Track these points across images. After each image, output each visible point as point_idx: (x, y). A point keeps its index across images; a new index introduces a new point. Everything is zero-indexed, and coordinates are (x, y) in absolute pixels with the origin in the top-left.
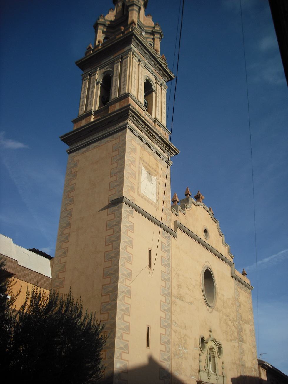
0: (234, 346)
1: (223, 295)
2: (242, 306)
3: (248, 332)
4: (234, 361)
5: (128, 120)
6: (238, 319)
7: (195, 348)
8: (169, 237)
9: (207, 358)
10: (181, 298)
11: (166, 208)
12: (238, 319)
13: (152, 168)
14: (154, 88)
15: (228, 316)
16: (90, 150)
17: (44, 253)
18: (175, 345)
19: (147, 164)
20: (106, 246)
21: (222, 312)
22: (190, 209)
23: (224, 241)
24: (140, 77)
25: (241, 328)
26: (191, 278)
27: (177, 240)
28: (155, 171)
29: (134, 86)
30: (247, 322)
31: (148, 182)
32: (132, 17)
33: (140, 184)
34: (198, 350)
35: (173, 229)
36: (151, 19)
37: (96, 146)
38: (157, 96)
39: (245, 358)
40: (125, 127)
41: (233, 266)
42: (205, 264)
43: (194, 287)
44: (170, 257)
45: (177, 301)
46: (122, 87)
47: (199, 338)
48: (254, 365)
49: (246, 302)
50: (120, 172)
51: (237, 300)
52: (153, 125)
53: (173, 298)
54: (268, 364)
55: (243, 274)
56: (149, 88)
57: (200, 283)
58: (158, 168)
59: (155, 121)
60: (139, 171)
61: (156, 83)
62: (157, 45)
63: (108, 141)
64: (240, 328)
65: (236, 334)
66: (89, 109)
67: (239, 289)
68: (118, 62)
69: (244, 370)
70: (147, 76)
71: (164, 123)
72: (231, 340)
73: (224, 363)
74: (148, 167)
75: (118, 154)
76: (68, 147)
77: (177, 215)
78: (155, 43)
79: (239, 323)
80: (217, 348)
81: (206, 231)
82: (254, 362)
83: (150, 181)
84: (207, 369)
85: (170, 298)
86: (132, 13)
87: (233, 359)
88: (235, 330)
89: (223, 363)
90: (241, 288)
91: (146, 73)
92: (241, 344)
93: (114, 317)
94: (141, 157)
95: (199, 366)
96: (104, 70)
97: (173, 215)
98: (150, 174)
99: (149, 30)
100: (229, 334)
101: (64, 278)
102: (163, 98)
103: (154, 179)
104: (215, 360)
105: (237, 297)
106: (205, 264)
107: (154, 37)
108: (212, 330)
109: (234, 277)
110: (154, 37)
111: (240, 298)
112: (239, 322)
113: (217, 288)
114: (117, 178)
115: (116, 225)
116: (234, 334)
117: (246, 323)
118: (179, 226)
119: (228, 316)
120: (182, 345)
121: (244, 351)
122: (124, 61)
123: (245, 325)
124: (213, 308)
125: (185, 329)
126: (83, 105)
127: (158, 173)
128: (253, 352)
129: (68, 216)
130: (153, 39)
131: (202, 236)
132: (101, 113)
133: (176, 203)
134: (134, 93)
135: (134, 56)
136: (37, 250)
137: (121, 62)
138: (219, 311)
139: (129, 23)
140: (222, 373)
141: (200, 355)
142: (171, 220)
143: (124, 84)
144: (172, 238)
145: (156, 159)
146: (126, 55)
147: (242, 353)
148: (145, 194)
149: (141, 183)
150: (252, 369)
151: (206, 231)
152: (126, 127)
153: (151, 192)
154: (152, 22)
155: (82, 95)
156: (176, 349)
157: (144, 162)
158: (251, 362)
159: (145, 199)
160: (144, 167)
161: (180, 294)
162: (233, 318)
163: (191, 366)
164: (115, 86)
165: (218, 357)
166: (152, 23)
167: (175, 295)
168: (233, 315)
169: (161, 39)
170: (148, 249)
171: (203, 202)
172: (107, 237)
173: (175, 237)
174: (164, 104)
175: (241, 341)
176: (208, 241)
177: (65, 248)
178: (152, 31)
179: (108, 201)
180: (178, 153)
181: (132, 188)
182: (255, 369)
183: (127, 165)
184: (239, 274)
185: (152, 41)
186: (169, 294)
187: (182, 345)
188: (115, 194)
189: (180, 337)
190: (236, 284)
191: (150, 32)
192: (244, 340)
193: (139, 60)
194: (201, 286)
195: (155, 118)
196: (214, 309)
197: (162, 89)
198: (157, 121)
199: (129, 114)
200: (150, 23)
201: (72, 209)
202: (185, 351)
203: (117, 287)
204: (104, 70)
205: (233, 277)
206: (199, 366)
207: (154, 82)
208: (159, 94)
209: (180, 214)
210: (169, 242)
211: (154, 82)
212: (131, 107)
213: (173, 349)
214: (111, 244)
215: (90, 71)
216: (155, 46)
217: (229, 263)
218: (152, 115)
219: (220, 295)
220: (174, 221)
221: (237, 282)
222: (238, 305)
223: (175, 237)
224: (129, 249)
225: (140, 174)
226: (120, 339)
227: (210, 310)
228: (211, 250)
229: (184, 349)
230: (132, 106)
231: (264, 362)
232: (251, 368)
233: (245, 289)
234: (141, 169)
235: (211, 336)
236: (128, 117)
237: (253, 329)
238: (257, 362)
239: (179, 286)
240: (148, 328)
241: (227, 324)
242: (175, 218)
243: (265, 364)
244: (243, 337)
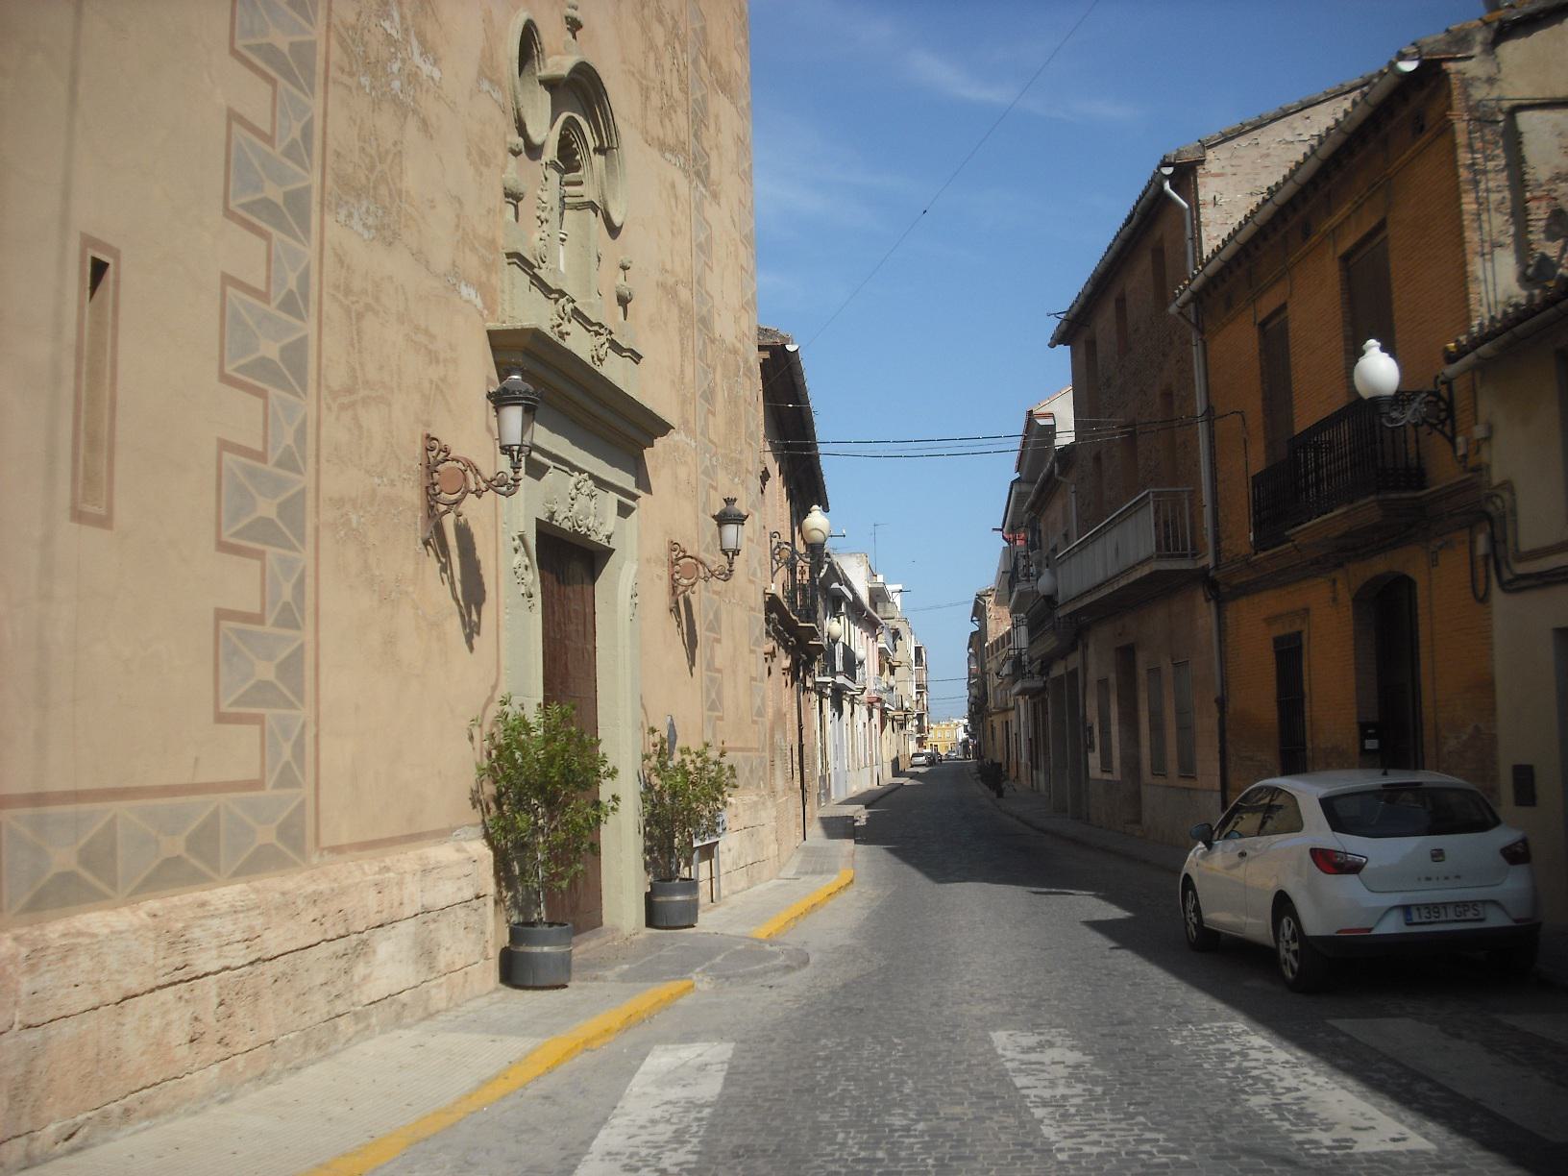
147: (700, 246)
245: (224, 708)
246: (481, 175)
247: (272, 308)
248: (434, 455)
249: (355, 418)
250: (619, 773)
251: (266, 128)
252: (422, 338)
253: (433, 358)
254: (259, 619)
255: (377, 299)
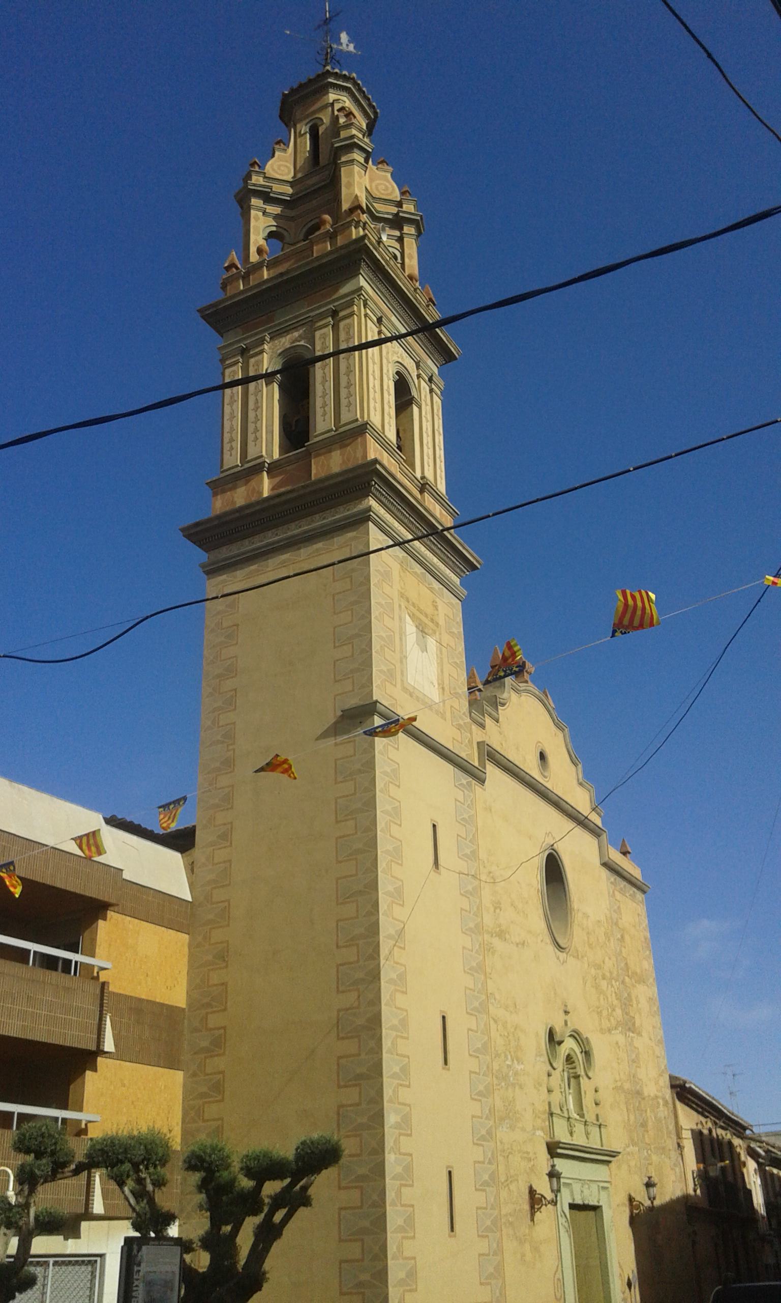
0: (617, 1043)
1: (586, 916)
2: (627, 937)
3: (644, 1004)
4: (619, 1084)
5: (370, 498)
6: (620, 971)
7: (538, 1058)
8: (469, 784)
9: (563, 1080)
10: (501, 934)
11: (460, 711)
12: (620, 971)
13: (426, 616)
14: (414, 393)
15: (598, 967)
16: (269, 569)
17: (132, 822)
18: (498, 1055)
19: (415, 607)
20: (337, 822)
21: (586, 959)
22: (507, 704)
23: (581, 776)
24: (385, 371)
25: (628, 995)
26: (518, 882)
27: (485, 790)
28: (432, 620)
29: (374, 399)
30: (641, 980)
31: (420, 653)
32: (350, 185)
33: (404, 660)
34: (544, 1062)
35: (476, 764)
36: (389, 175)
37: (284, 561)
38: (423, 413)
39: (642, 1074)
40: (365, 517)
41: (604, 837)
42: (544, 841)
43: (527, 903)
44: (474, 835)
45: (496, 941)
46: (344, 402)
47: (544, 1031)
48: (663, 1089)
49: (634, 926)
50: (361, 636)
51: (616, 924)
52: (419, 496)
53: (486, 937)
54: (694, 1085)
55: (621, 853)
56: (402, 388)
57: (538, 889)
58: (436, 612)
59: (424, 486)
60: (401, 628)
61: (419, 376)
62: (411, 257)
63: (317, 550)
64: (626, 995)
65: (619, 1012)
66: (252, 453)
67: (618, 896)
68: (327, 326)
69: (643, 1105)
70: (398, 362)
71: (442, 487)
72: (609, 1031)
73: (600, 1091)
74: (418, 614)
75: (349, 588)
76: (201, 556)
77: (482, 726)
78: (407, 251)
79: (623, 982)
80: (582, 1052)
81: (542, 756)
82: (661, 1083)
83: (424, 649)
84: (565, 1109)
85: (480, 939)
86: (351, 174)
87: (618, 1079)
88: (616, 1002)
89: (596, 1091)
90: (622, 891)
91: (394, 352)
92: (632, 1037)
93: (376, 1000)
94: (403, 591)
95: (549, 1104)
96: (285, 342)
97: (474, 727)
98: (422, 630)
99: (388, 213)
100: (605, 1013)
101: (228, 901)
102: (436, 416)
103: (431, 642)
104: (579, 1084)
105: (615, 916)
106: (544, 841)
107: (402, 234)
108: (569, 1009)
109: (608, 866)
110: (402, 234)
111: (621, 919)
112: (624, 979)
113: (572, 899)
114: (353, 651)
115: (360, 771)
116: (614, 1013)
117: (638, 982)
118: (491, 755)
119: (598, 967)
120: (512, 1053)
121: (637, 1055)
122: (342, 324)
123: (636, 986)
124: (567, 950)
125: (515, 1012)
126: (234, 438)
127: (437, 625)
128: (658, 1057)
129: (223, 742)
130: (400, 240)
131: (532, 767)
132: (288, 468)
133: (476, 695)
134: (375, 420)
135: (368, 311)
136: (129, 822)
137: (335, 327)
138: (580, 957)
139: (345, 206)
140: (597, 1116)
141: (549, 1075)
142: (470, 742)
143: (350, 395)
144: (476, 787)
145: (431, 589)
146: (349, 307)
147: (634, 1061)
148: (416, 686)
149: (406, 657)
150: (659, 1100)
151: (542, 756)
152: (368, 518)
153: (428, 678)
154: (393, 187)
155: (227, 409)
156: (500, 1065)
157: (408, 602)
158: (657, 1083)
159: (418, 699)
160: (410, 616)
161: (500, 926)
162: (611, 972)
163: (533, 1104)
164: (324, 397)
165: (585, 1077)
166: (393, 189)
167: (490, 930)
168: (609, 964)
169: (419, 233)
170: (430, 821)
171: (534, 682)
172: (338, 800)
173: (482, 781)
174: (439, 434)
175: (629, 1029)
176: (548, 781)
177: (225, 824)
178: (397, 215)
179: (335, 711)
180: (479, 566)
181: (390, 675)
182: (664, 1099)
183: (376, 617)
184: (615, 856)
185: (398, 246)
186: (478, 929)
187: (512, 1053)
188: (350, 691)
189: (506, 1034)
190: (612, 883)
191: (390, 217)
192: (636, 1026)
193: (380, 320)
194: (540, 897)
195: (423, 478)
196: (568, 952)
197: (431, 391)
198: (427, 486)
199: (373, 483)
200: (387, 188)
201: (234, 723)
202: (519, 1067)
203: (376, 924)
204: (285, 342)
205: (605, 865)
206: (549, 1104)
207: (414, 374)
208: (426, 409)
209: (488, 721)
210: (470, 796)
211: (414, 374)
212: (378, 466)
213: (496, 1067)
214: (352, 819)
215: (245, 339)
216: (407, 260)
217: (595, 832)
218: (414, 471)
219: (580, 915)
220: (478, 743)
221: (613, 878)
222: (619, 936)
223: (482, 781)
224: (394, 829)
225: (402, 633)
226: (392, 1054)
227: (562, 956)
228: (557, 804)
229: (515, 1061)
230: (380, 464)
231: (685, 1082)
232: (657, 1097)
233: (631, 892)
234: (405, 623)
235: (569, 1023)
236: (370, 486)
237: (653, 995)
238: (668, 1083)
239: (497, 906)
240: (444, 1017)
241: (597, 987)
242: (478, 735)
243: (687, 1085)
244: (634, 1018)
245: (482, 1281)
246: (539, 1090)
247: (467, 842)
248: (532, 1192)
249: (509, 1188)
250: (303, 1138)
251: (463, 802)
252: (525, 1155)
253: (530, 1160)
254: (488, 1255)
255: (512, 1149)
